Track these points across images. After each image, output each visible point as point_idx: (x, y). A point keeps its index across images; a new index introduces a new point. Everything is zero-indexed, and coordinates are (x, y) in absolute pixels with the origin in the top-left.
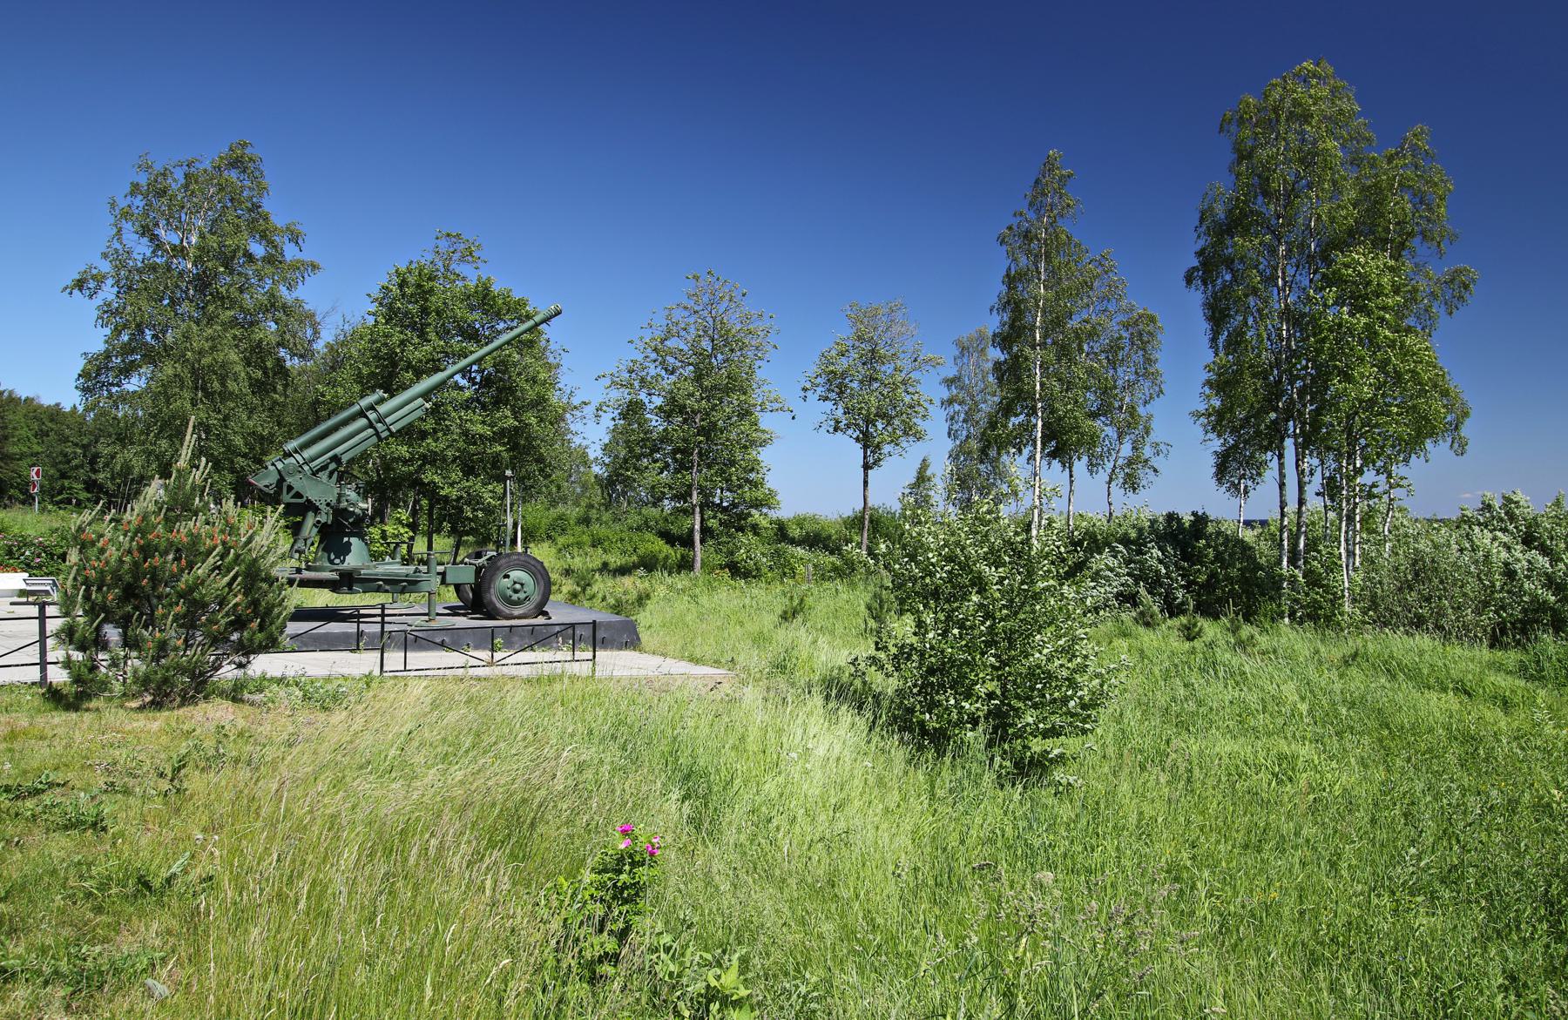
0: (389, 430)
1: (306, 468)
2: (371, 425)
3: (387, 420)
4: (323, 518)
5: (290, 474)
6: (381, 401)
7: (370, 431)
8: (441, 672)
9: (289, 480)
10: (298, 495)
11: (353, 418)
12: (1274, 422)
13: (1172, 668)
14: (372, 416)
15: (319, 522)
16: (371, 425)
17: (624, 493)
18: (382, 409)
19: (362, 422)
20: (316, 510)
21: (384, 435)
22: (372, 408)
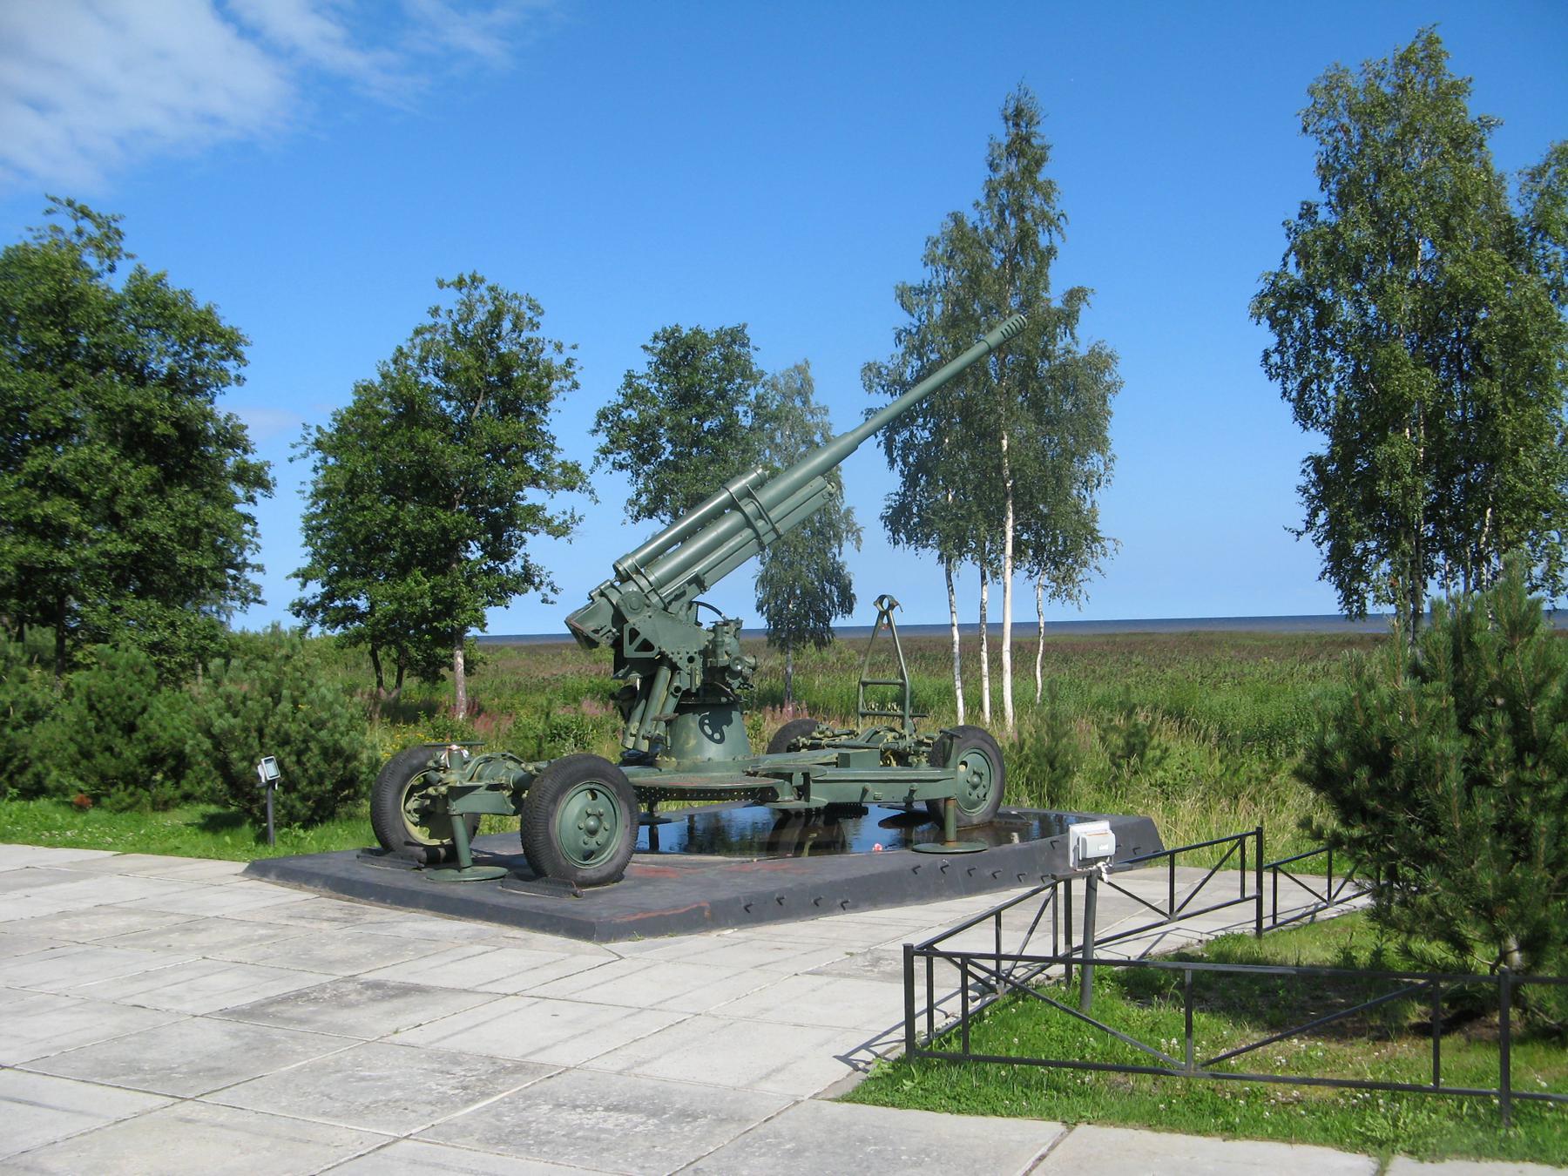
0: (774, 529)
1: (655, 599)
2: (748, 523)
3: (772, 515)
4: (683, 682)
5: (635, 611)
6: (760, 484)
7: (748, 532)
8: (222, 1084)
9: (633, 620)
10: (647, 646)
11: (717, 515)
12: (1447, 979)
13: (929, 729)
14: (749, 509)
15: (678, 689)
16: (748, 523)
17: (1351, 502)
18: (765, 496)
19: (731, 521)
20: (674, 668)
21: (767, 539)
22: (748, 494)
